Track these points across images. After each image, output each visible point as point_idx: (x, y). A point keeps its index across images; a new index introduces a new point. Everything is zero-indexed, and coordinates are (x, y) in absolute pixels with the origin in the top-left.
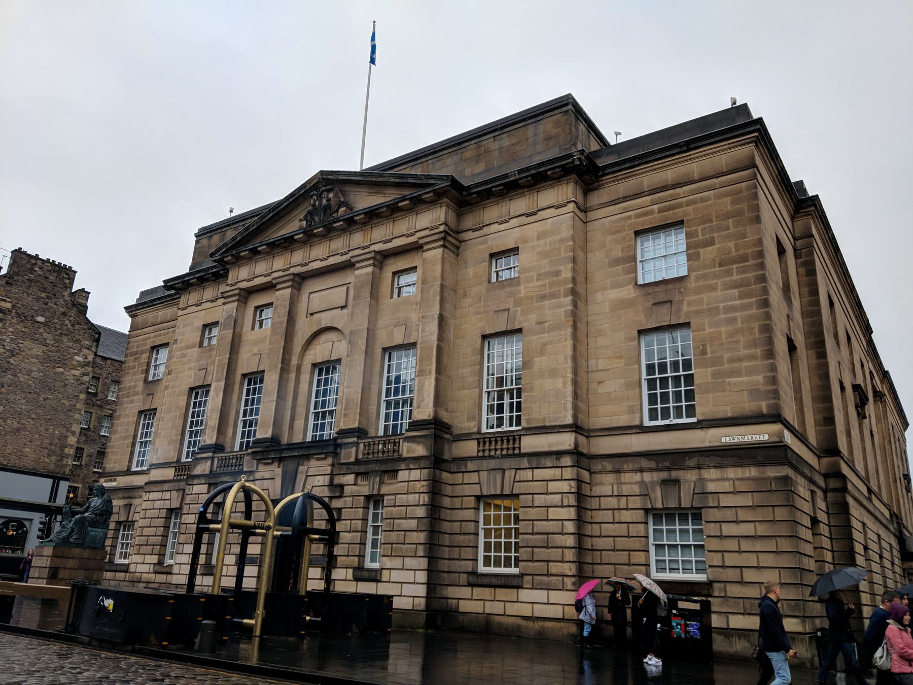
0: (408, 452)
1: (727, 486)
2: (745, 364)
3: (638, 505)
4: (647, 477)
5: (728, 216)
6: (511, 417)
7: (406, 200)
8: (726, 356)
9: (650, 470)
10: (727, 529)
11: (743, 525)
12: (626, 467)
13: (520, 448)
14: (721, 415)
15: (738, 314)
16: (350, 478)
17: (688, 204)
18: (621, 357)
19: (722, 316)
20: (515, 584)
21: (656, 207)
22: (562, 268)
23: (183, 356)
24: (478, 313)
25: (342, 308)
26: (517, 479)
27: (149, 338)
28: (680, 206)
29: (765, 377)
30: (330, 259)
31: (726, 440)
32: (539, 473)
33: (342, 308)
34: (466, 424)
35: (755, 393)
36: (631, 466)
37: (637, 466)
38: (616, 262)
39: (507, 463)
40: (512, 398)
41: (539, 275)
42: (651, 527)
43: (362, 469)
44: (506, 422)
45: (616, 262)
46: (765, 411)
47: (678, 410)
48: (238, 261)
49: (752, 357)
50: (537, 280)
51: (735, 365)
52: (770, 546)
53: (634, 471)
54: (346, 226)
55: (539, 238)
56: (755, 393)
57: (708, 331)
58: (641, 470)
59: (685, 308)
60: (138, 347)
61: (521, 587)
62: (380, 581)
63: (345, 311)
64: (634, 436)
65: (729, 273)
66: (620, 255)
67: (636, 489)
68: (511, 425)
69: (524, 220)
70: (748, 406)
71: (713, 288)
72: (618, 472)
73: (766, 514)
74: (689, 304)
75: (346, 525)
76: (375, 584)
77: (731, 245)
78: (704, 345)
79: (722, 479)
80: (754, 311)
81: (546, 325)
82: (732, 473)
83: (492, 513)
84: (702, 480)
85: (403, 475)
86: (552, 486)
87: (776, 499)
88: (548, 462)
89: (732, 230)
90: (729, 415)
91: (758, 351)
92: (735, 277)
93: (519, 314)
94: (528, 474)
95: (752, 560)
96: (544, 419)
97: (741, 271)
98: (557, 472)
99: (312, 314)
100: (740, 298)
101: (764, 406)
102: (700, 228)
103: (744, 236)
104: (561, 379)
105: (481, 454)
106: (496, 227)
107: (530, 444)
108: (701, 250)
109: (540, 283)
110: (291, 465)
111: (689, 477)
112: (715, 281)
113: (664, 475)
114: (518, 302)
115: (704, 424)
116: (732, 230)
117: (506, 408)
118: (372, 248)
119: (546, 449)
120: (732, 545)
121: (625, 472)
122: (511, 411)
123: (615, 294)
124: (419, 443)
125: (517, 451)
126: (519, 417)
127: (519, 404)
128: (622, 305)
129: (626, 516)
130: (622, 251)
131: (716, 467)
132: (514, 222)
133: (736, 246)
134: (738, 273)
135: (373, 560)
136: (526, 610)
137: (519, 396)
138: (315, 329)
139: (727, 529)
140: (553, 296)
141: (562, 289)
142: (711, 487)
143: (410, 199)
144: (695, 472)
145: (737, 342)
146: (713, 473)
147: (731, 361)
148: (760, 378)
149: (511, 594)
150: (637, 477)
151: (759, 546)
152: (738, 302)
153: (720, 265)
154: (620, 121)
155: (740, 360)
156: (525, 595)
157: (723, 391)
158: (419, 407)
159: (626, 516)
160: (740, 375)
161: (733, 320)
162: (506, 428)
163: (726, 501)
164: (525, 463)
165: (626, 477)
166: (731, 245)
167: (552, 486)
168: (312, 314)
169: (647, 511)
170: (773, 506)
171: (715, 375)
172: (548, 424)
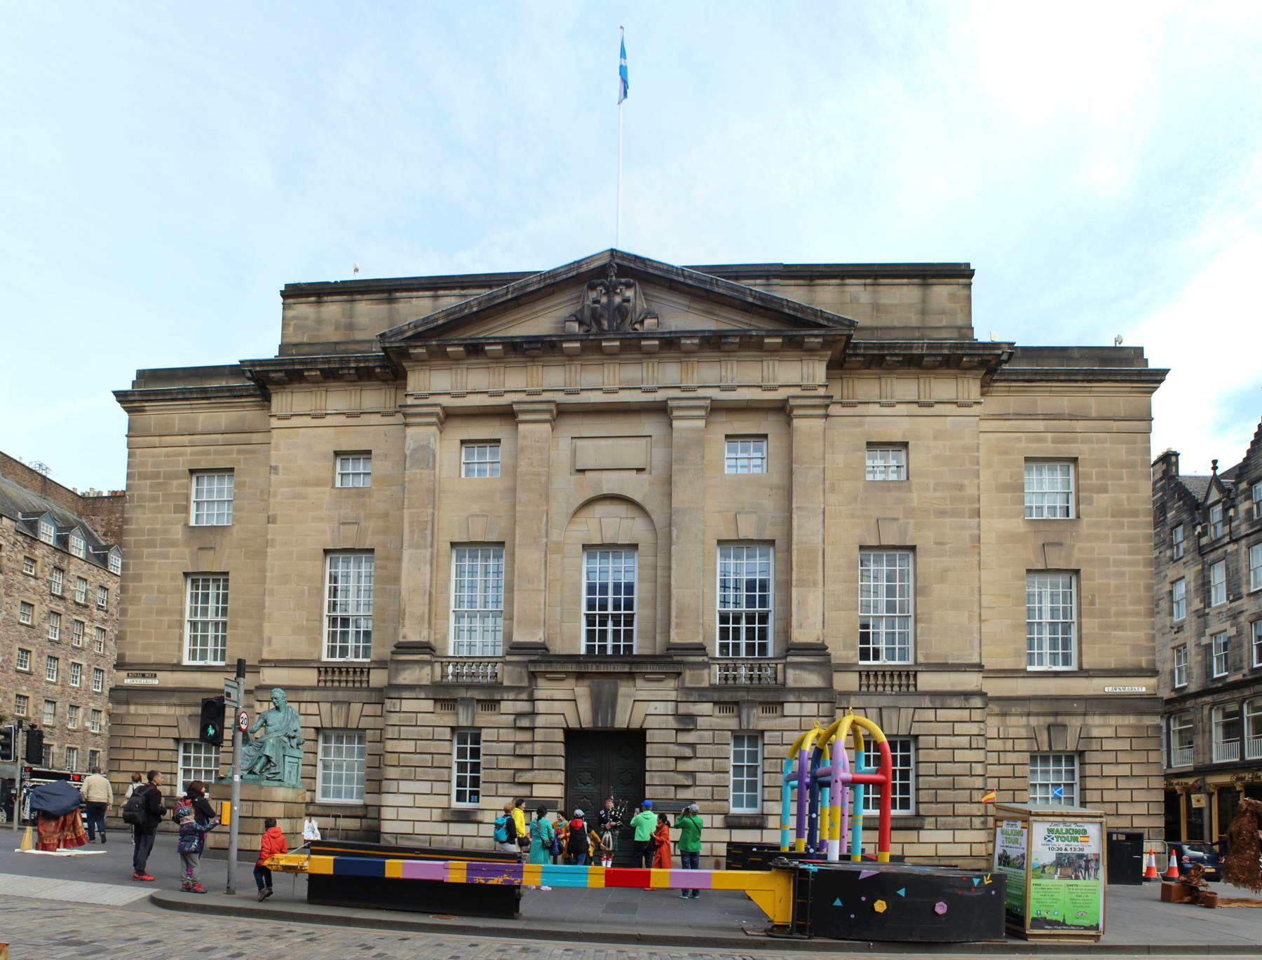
0: (795, 681)
1: (1109, 732)
2: (1129, 619)
3: (1025, 748)
4: (1033, 721)
5: (1122, 465)
6: (216, 651)
7: (576, 341)
8: (1113, 609)
9: (1038, 714)
10: (1107, 770)
11: (1121, 767)
12: (1013, 710)
13: (915, 686)
14: (1106, 666)
15: (1127, 569)
16: (706, 708)
17: (1083, 442)
18: (1008, 596)
19: (1112, 569)
20: (917, 825)
21: (1049, 435)
22: (966, 482)
23: (297, 496)
24: (853, 516)
25: (639, 470)
26: (916, 718)
27: (181, 454)
28: (1074, 441)
29: (1146, 635)
30: (622, 393)
31: (1109, 690)
32: (942, 714)
33: (639, 470)
34: (843, 653)
35: (1136, 648)
36: (1019, 710)
37: (1026, 710)
38: (1004, 488)
39: (903, 702)
40: (217, 631)
41: (936, 485)
42: (181, 754)
43: (727, 697)
44: (210, 655)
45: (1004, 488)
46: (1144, 665)
47: (1054, 657)
48: (439, 357)
49: (1136, 614)
50: (935, 490)
51: (1121, 619)
52: (1142, 783)
53: (1021, 715)
54: (427, 357)
55: (935, 438)
56: (1136, 648)
57: (1097, 581)
58: (1029, 715)
59: (1076, 554)
60: (155, 465)
61: (922, 828)
62: (766, 828)
63: (644, 476)
64: (1020, 680)
65: (1121, 526)
66: (1009, 480)
67: (1023, 733)
68: (215, 659)
69: (915, 409)
70: (1130, 660)
71: (1105, 538)
72: (1004, 715)
73: (1141, 757)
74: (1080, 550)
75: (705, 764)
76: (759, 832)
77: (1124, 496)
78: (1093, 596)
79: (1105, 726)
80: (1141, 569)
81: (948, 547)
82: (1114, 720)
83: (746, 749)
84: (1084, 726)
85: (790, 708)
86: (959, 728)
87: (1150, 744)
88: (955, 702)
89: (1124, 482)
90: (1113, 666)
91: (1142, 608)
92: (1126, 531)
93: (911, 527)
94: (930, 714)
95: (1126, 796)
96: (946, 656)
97: (1133, 526)
98: (965, 714)
99: (583, 471)
100: (1130, 553)
101: (1144, 661)
102: (1094, 471)
103: (1136, 490)
104: (966, 614)
105: (322, 684)
106: (875, 409)
107: (927, 681)
108: (1095, 496)
109: (938, 494)
110: (606, 685)
111: (1075, 722)
112: (1106, 532)
113: (1051, 720)
114: (910, 512)
115: (1082, 673)
116: (1124, 482)
117: (211, 641)
118: (701, 393)
119: (948, 688)
120: (1111, 783)
121: (1012, 715)
122: (216, 645)
123: (1002, 525)
124: (811, 671)
125: (365, 685)
126: (223, 651)
127: (224, 637)
128: (1010, 538)
129: (1012, 758)
130: (1011, 476)
131: (1100, 714)
132: (901, 409)
133: (1128, 499)
134: (1129, 528)
135: (325, 794)
136: (929, 850)
137: (224, 630)
138: (590, 494)
139: (1107, 770)
140: (955, 513)
141: (967, 507)
142: (1096, 732)
143: (465, 346)
144: (1080, 718)
145: (1124, 596)
146: (1095, 720)
147: (1118, 614)
148: (1141, 634)
149: (912, 835)
150: (1024, 720)
151: (1133, 784)
152: (1127, 557)
153: (1113, 516)
154: (999, 316)
155: (1125, 614)
156: (925, 835)
157: (1109, 643)
158: (801, 626)
159: (1012, 758)
160: (1125, 630)
161: (1121, 575)
162: (350, 658)
163: (1107, 745)
164: (927, 702)
165: (1012, 720)
166: (1124, 496)
167: (959, 728)
168: (583, 471)
169: (177, 740)
170: (433, 740)
171: (1102, 626)
172: (950, 661)
